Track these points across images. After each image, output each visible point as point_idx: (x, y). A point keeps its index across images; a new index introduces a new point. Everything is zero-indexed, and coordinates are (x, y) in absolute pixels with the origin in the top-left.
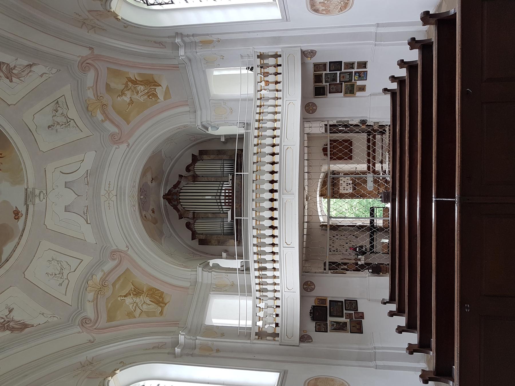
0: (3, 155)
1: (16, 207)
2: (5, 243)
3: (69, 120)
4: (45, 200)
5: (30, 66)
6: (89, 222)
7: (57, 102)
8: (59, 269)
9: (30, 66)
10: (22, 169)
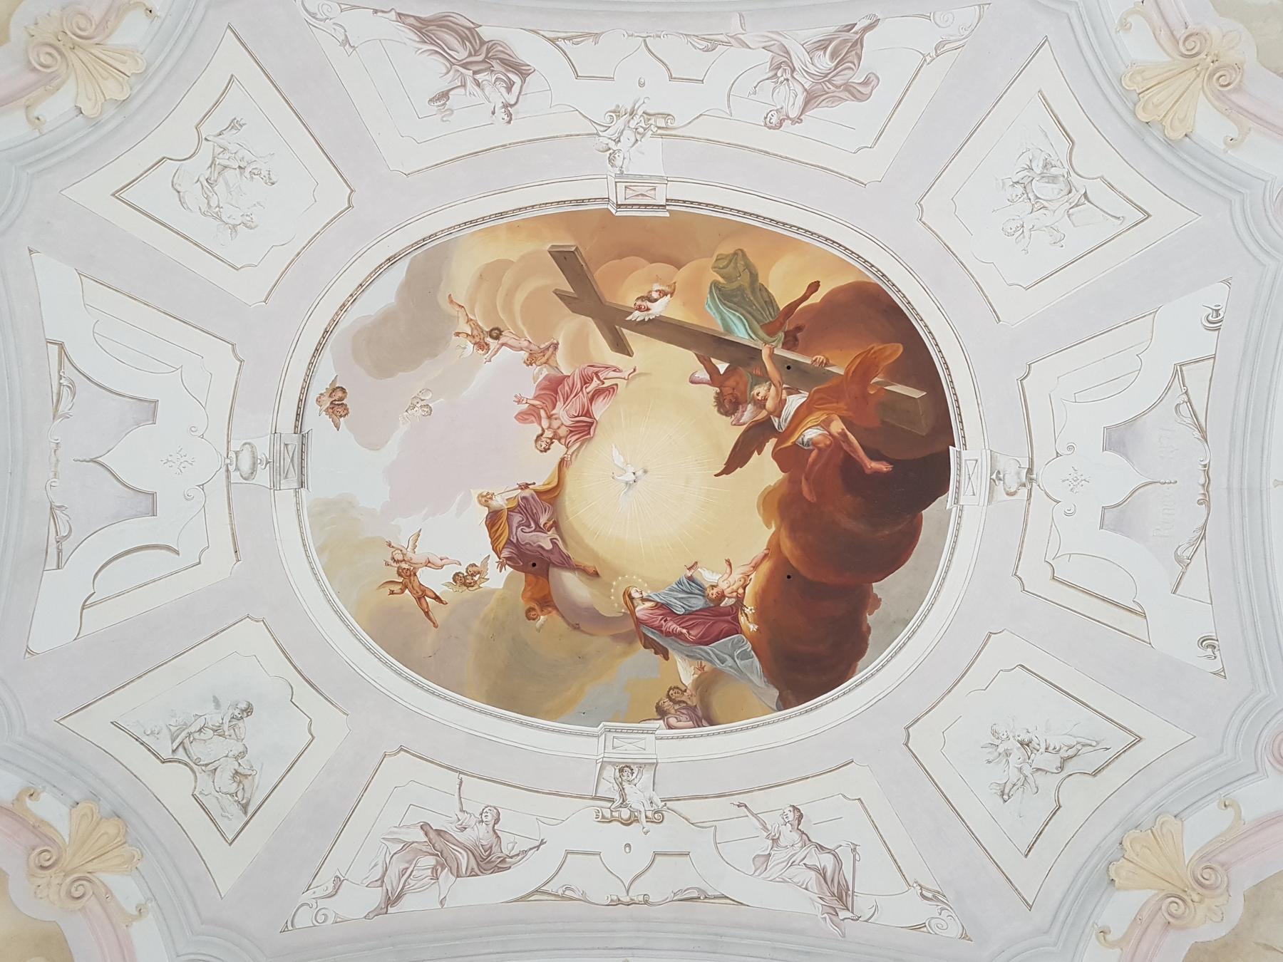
0: (387, 590)
1: (338, 428)
2: (387, 318)
3: (181, 754)
4: (235, 446)
5: (391, 900)
6: (54, 350)
7: (245, 808)
8: (219, 188)
9: (391, 900)
10: (320, 551)
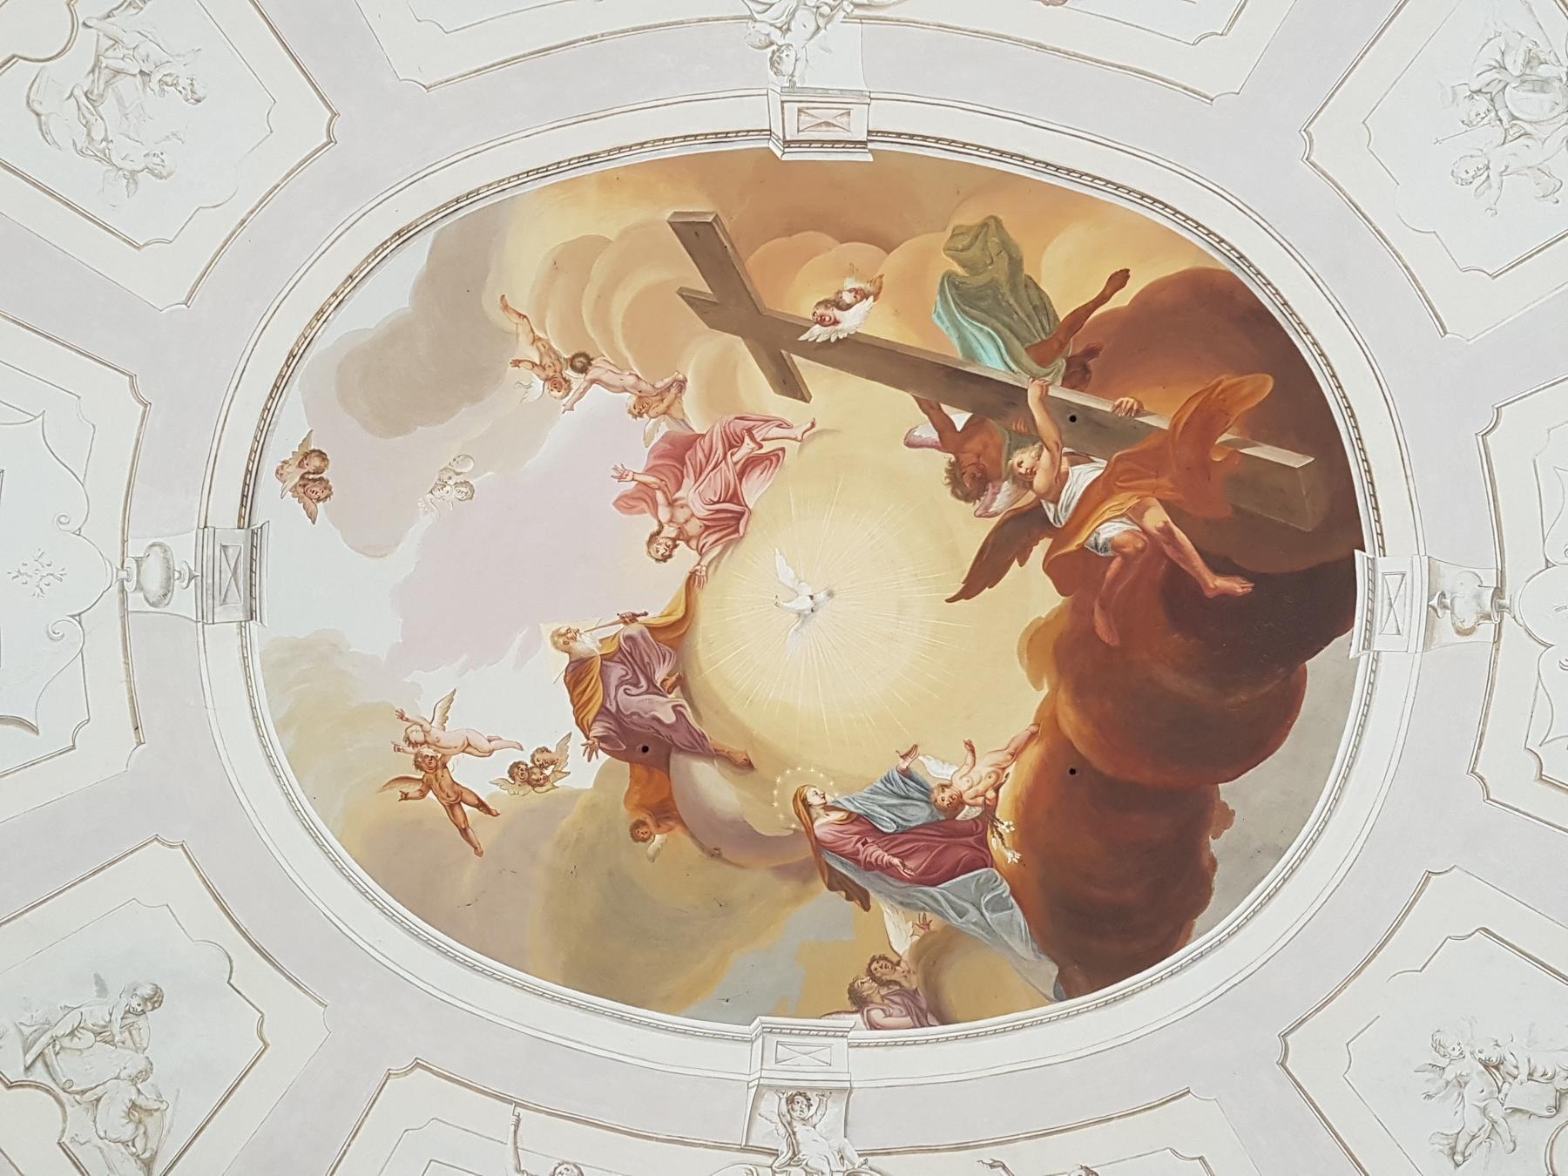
0: (396, 792)
2: (395, 334)
3: (39, 1074)
4: (135, 549)
8: (108, 107)
10: (282, 727)
